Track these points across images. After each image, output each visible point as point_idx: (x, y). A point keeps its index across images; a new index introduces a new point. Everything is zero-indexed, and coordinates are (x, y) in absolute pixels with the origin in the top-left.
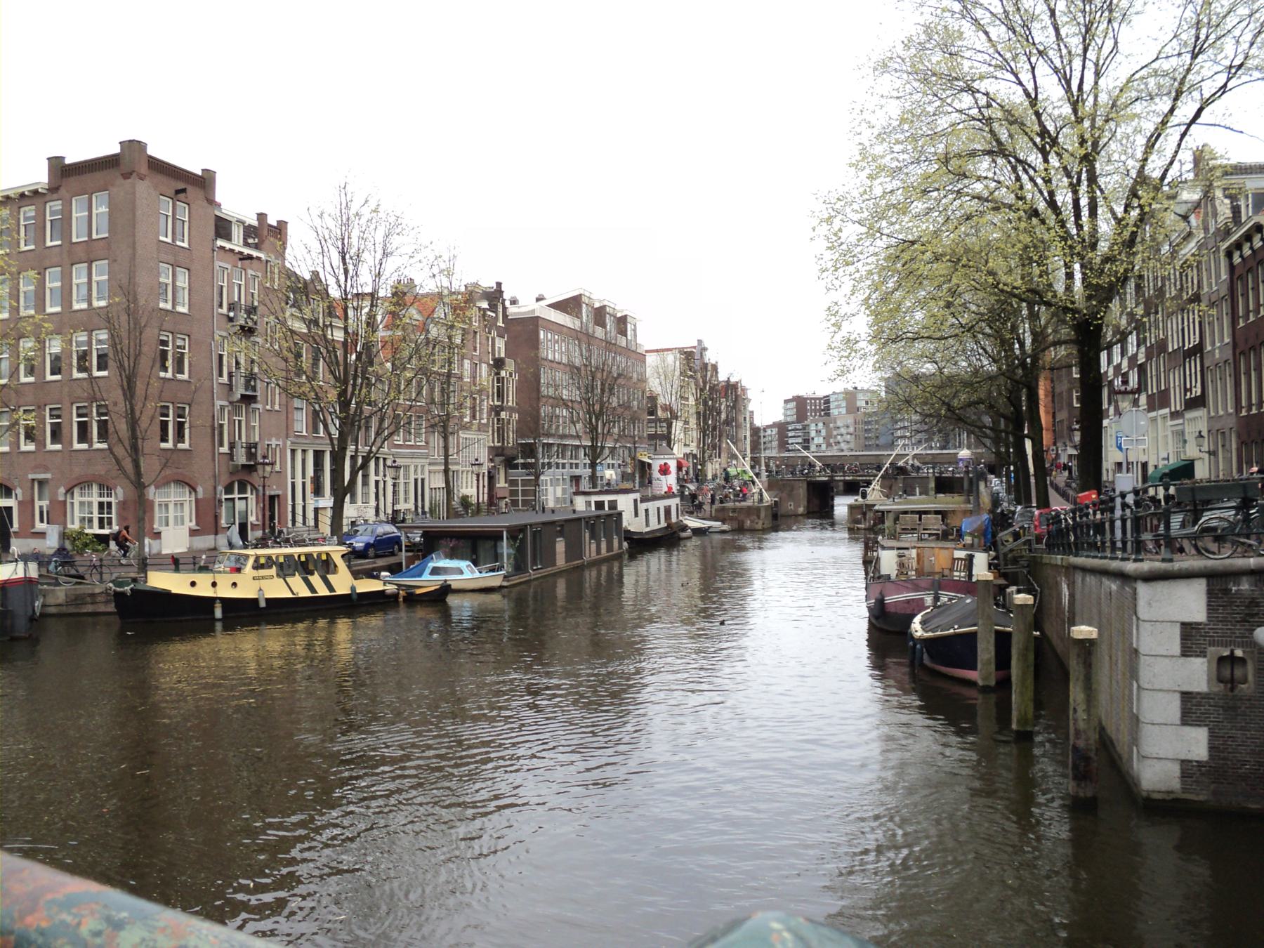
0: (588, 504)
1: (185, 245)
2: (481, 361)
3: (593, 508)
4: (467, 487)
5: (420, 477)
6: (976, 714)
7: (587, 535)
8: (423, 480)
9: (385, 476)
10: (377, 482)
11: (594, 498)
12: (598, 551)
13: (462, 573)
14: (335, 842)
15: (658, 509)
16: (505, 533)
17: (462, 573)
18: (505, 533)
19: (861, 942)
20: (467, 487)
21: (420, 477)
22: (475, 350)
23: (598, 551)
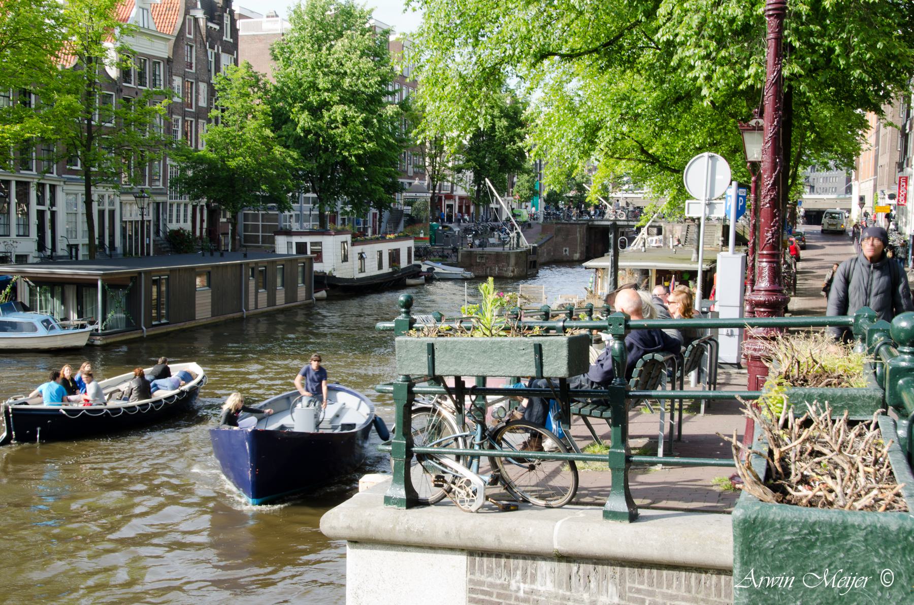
0: (289, 244)
1: (192, 37)
2: (197, 80)
3: (294, 252)
4: (178, 221)
5: (107, 207)
6: (790, 473)
7: (252, 283)
8: (112, 213)
9: (53, 204)
10: (41, 214)
11: (296, 239)
12: (272, 300)
13: (35, 329)
14: (168, 492)
15: (380, 253)
16: (100, 283)
17: (35, 329)
18: (100, 283)
19: (911, 76)
20: (178, 221)
21: (107, 207)
22: (191, 68)
23: (272, 300)
